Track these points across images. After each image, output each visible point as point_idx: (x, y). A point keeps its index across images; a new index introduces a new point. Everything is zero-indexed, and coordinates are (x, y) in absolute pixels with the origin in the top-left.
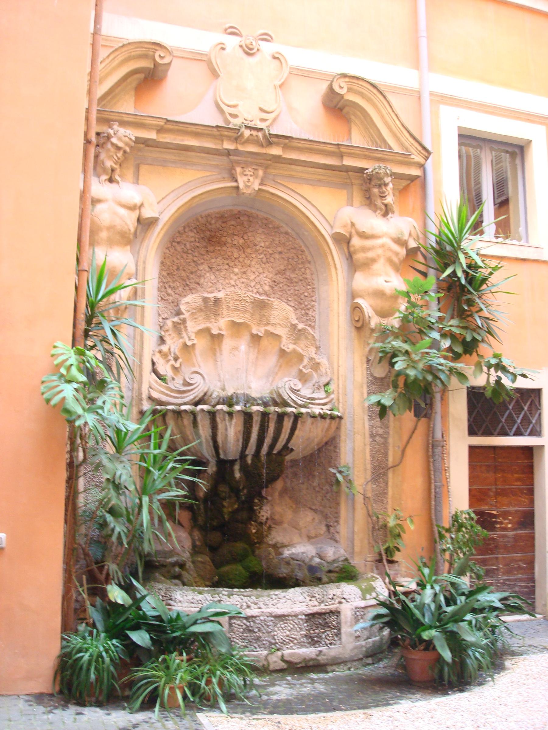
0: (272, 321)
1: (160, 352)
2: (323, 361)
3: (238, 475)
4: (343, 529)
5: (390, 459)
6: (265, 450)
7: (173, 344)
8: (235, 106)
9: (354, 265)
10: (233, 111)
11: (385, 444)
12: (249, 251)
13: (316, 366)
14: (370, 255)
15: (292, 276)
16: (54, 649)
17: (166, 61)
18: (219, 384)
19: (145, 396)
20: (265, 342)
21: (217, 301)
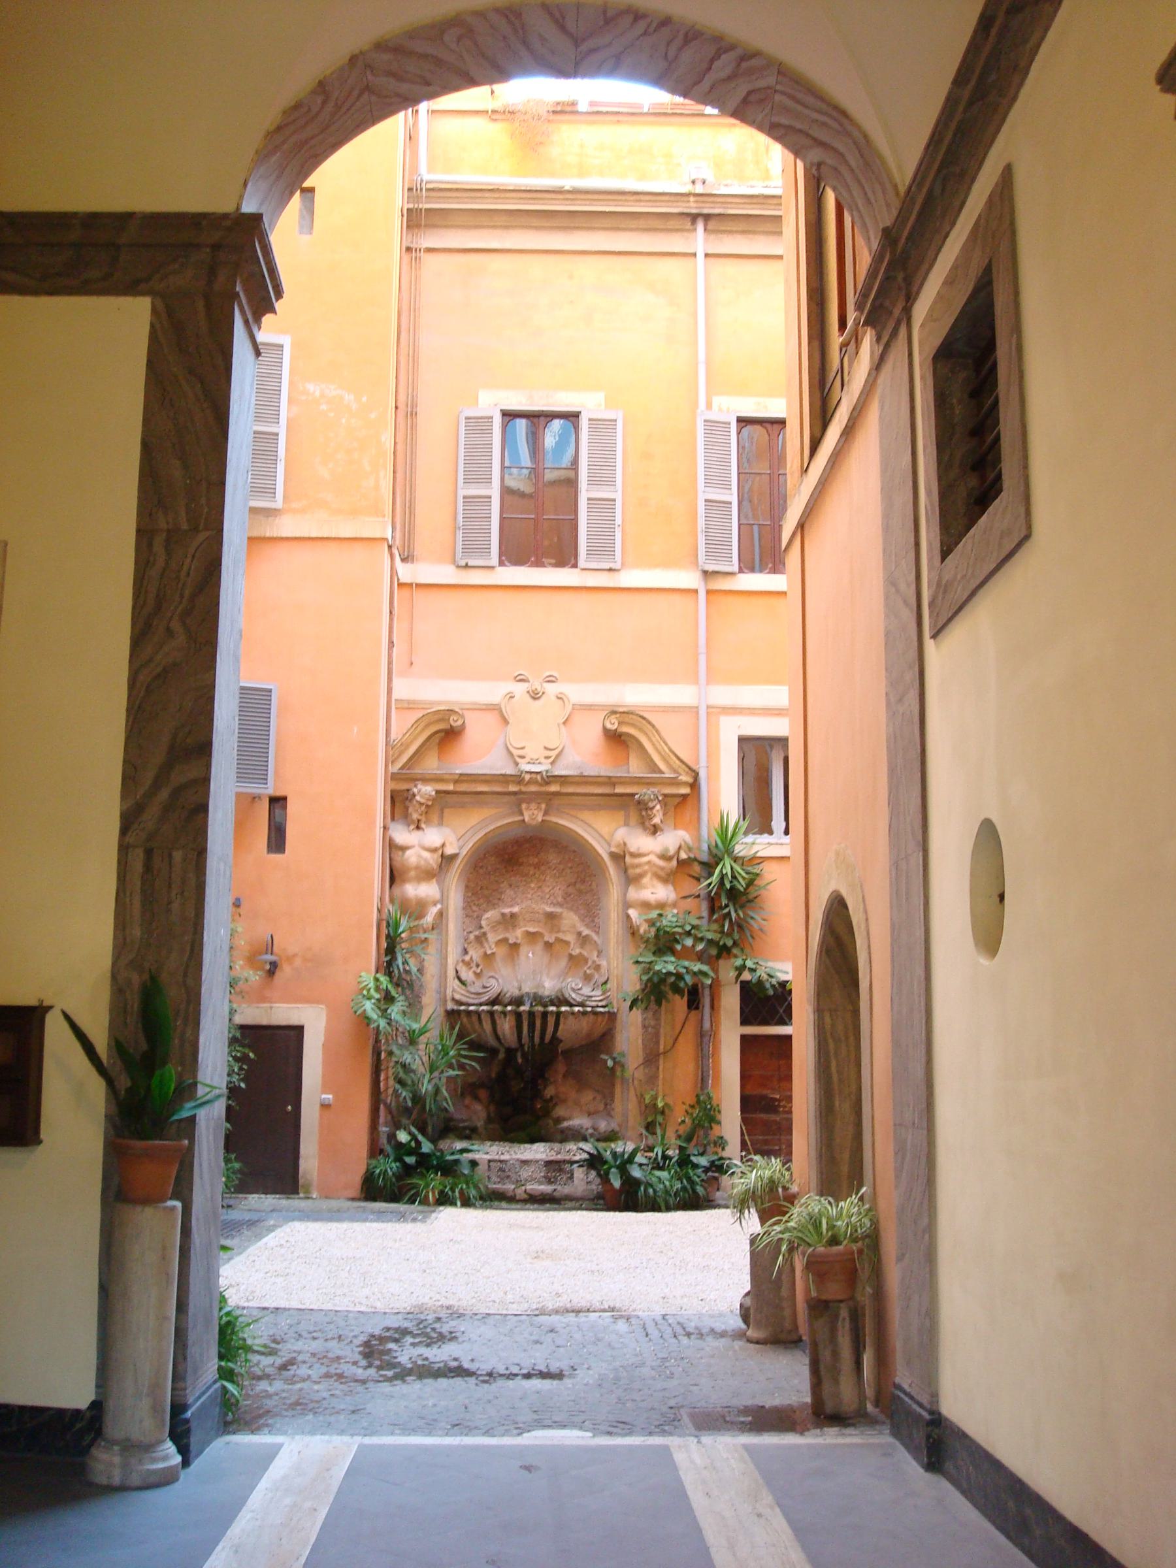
0: (563, 929)
1: (463, 961)
2: (604, 963)
3: (520, 1060)
4: (618, 1106)
5: (662, 1047)
6: (537, 1040)
7: (475, 954)
8: (523, 748)
9: (631, 879)
10: (521, 752)
11: (657, 1035)
12: (543, 868)
13: (598, 968)
14: (638, 871)
15: (582, 887)
16: (362, 1170)
17: (460, 722)
18: (516, 984)
19: (449, 997)
20: (557, 947)
21: (513, 915)
